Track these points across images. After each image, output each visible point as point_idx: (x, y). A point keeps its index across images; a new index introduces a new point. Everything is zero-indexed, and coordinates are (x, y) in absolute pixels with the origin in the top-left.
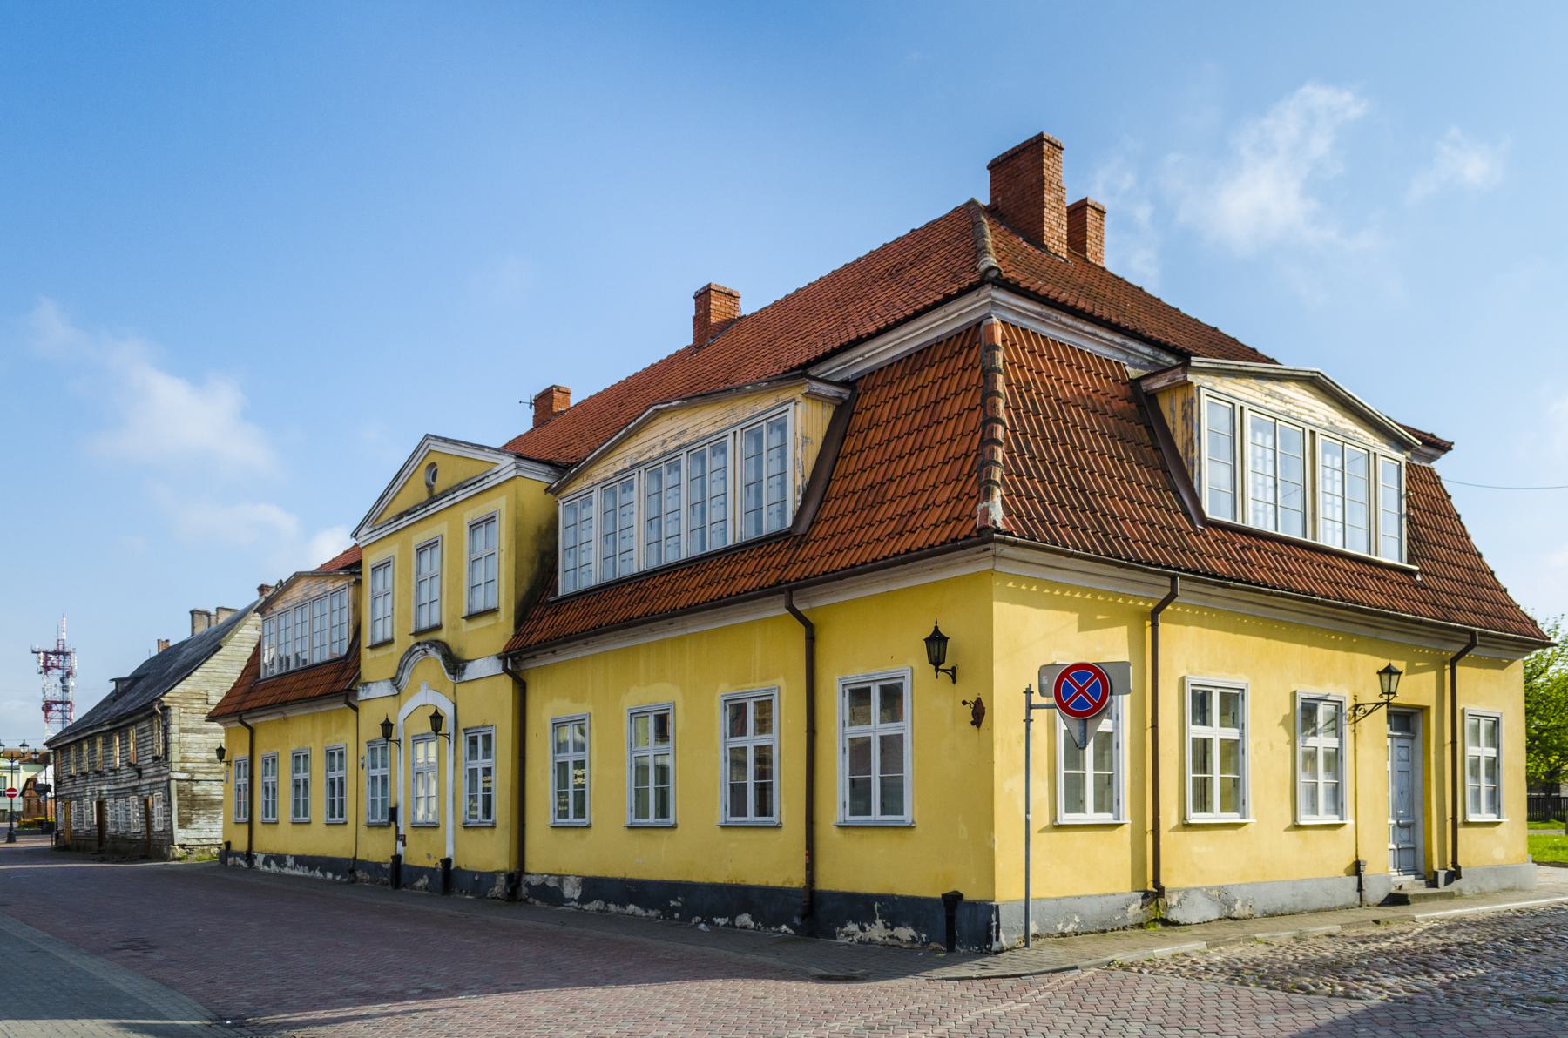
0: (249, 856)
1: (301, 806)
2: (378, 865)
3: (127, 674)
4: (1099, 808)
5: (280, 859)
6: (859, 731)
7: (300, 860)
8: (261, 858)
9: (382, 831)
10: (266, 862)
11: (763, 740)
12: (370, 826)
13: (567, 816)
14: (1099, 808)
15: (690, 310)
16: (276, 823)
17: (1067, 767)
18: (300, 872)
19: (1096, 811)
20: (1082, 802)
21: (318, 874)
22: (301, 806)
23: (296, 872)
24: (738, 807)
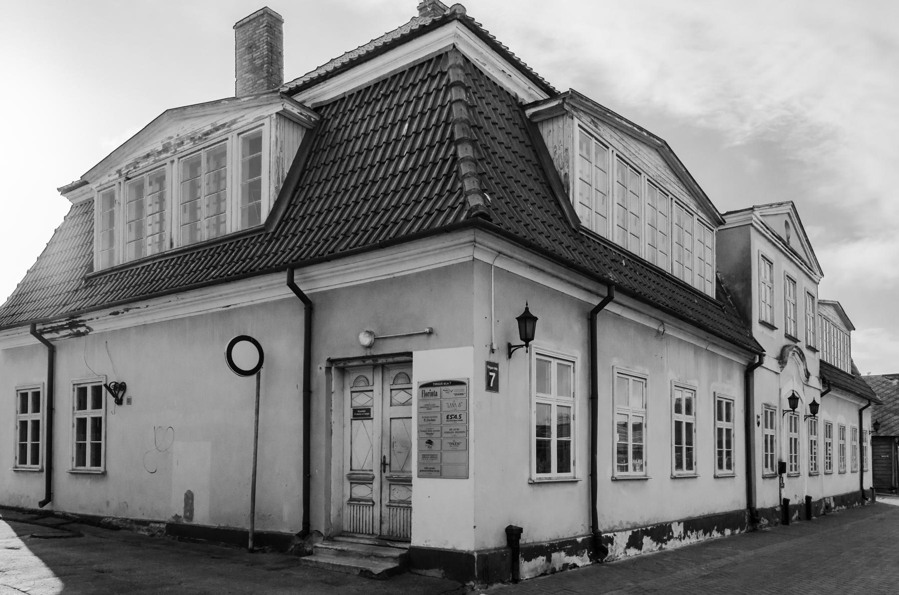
0: (596, 544)
1: (684, 457)
2: (773, 509)
3: (584, 223)
4: (560, 470)
5: (660, 532)
6: (81, 414)
7: (691, 525)
8: (622, 539)
9: (772, 481)
10: (635, 541)
11: (81, 414)
12: (764, 477)
13: (627, 470)
14: (560, 470)
15: (779, 351)
16: (104, 474)
17: (85, 444)
18: (693, 539)
19: (559, 472)
20: (550, 466)
21: (716, 535)
22: (684, 457)
23: (686, 542)
24: (543, 465)
